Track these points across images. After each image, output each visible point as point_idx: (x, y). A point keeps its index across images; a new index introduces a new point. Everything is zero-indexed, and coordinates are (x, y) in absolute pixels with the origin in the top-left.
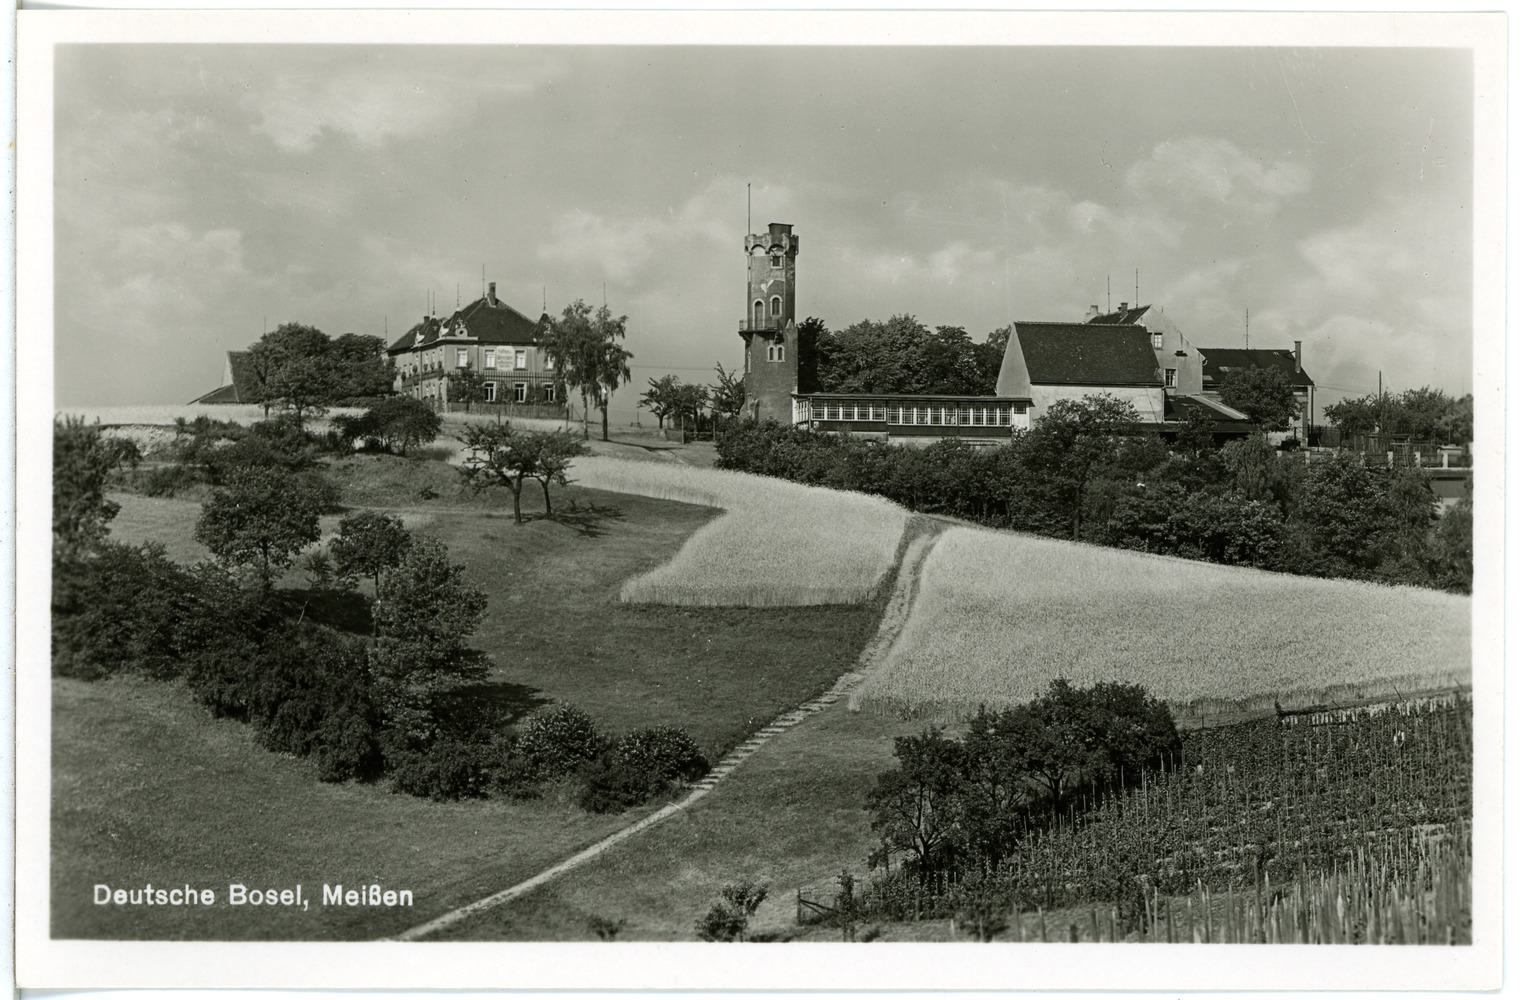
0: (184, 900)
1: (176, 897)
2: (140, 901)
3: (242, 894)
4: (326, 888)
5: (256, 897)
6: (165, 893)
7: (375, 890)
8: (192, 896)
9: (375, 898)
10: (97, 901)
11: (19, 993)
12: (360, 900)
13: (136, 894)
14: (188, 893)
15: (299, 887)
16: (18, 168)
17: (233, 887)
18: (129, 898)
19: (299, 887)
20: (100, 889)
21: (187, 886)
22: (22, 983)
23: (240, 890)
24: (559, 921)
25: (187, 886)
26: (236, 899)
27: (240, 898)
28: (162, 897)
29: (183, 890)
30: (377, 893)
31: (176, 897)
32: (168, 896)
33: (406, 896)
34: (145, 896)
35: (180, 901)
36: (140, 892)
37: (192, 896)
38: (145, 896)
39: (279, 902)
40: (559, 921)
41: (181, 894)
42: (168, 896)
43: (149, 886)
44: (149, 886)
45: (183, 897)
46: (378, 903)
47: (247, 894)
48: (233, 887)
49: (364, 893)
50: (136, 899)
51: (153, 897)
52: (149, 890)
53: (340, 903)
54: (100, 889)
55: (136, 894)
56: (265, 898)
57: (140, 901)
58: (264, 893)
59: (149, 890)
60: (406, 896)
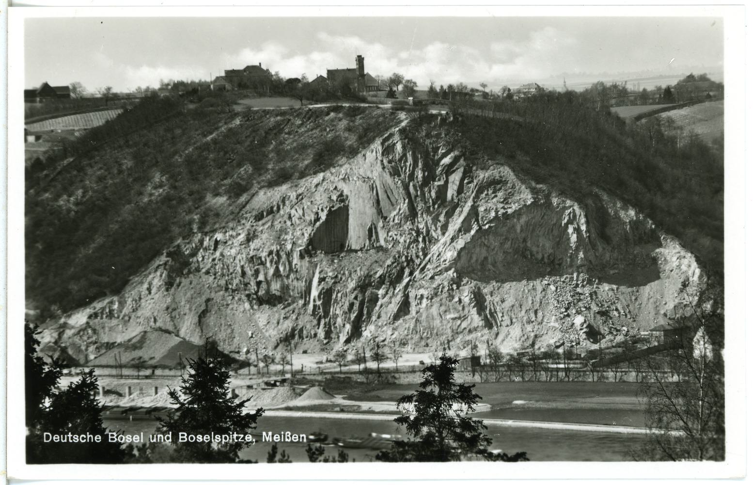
0: (87, 440)
1: (83, 438)
2: (66, 441)
3: (185, 437)
4: (264, 434)
5: (192, 438)
6: (78, 436)
7: (288, 434)
8: (90, 438)
9: (288, 438)
10: (45, 441)
11: (8, 481)
12: (140, 439)
13: (160, 439)
14: (89, 436)
15: (142, 433)
16: (9, 169)
17: (180, 433)
18: (60, 439)
19: (142, 433)
20: (46, 435)
21: (88, 433)
22: (10, 475)
23: (184, 435)
24: (461, 407)
25: (88, 433)
26: (182, 439)
27: (184, 439)
28: (76, 439)
29: (86, 435)
30: (289, 436)
31: (83, 438)
32: (79, 438)
33: (161, 437)
34: (68, 438)
35: (85, 440)
36: (66, 436)
37: (90, 438)
38: (68, 438)
39: (203, 440)
40: (461, 407)
41: (85, 437)
42: (79, 438)
43: (70, 433)
44: (70, 433)
45: (86, 438)
46: (289, 440)
47: (187, 437)
48: (180, 433)
49: (282, 436)
50: (64, 439)
51: (72, 438)
52: (70, 435)
53: (271, 440)
54: (46, 435)
55: (160, 439)
56: (196, 439)
57: (66, 441)
58: (196, 436)
59: (70, 435)
60: (161, 437)
